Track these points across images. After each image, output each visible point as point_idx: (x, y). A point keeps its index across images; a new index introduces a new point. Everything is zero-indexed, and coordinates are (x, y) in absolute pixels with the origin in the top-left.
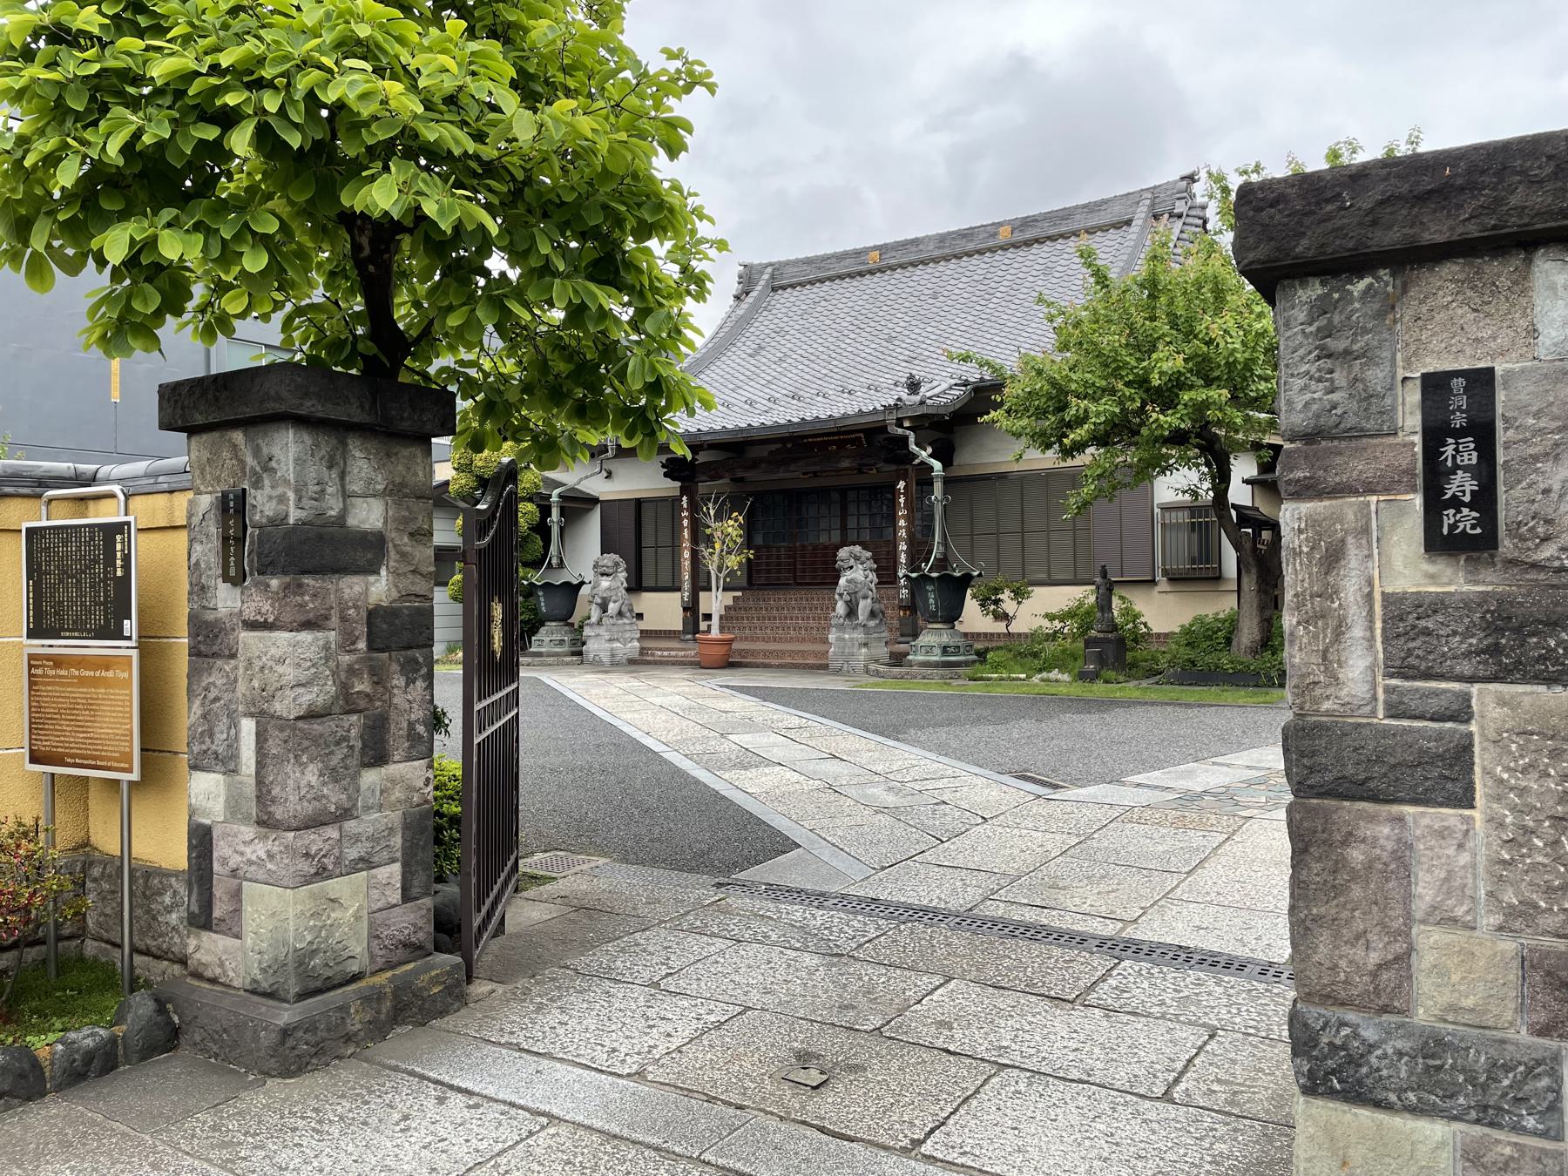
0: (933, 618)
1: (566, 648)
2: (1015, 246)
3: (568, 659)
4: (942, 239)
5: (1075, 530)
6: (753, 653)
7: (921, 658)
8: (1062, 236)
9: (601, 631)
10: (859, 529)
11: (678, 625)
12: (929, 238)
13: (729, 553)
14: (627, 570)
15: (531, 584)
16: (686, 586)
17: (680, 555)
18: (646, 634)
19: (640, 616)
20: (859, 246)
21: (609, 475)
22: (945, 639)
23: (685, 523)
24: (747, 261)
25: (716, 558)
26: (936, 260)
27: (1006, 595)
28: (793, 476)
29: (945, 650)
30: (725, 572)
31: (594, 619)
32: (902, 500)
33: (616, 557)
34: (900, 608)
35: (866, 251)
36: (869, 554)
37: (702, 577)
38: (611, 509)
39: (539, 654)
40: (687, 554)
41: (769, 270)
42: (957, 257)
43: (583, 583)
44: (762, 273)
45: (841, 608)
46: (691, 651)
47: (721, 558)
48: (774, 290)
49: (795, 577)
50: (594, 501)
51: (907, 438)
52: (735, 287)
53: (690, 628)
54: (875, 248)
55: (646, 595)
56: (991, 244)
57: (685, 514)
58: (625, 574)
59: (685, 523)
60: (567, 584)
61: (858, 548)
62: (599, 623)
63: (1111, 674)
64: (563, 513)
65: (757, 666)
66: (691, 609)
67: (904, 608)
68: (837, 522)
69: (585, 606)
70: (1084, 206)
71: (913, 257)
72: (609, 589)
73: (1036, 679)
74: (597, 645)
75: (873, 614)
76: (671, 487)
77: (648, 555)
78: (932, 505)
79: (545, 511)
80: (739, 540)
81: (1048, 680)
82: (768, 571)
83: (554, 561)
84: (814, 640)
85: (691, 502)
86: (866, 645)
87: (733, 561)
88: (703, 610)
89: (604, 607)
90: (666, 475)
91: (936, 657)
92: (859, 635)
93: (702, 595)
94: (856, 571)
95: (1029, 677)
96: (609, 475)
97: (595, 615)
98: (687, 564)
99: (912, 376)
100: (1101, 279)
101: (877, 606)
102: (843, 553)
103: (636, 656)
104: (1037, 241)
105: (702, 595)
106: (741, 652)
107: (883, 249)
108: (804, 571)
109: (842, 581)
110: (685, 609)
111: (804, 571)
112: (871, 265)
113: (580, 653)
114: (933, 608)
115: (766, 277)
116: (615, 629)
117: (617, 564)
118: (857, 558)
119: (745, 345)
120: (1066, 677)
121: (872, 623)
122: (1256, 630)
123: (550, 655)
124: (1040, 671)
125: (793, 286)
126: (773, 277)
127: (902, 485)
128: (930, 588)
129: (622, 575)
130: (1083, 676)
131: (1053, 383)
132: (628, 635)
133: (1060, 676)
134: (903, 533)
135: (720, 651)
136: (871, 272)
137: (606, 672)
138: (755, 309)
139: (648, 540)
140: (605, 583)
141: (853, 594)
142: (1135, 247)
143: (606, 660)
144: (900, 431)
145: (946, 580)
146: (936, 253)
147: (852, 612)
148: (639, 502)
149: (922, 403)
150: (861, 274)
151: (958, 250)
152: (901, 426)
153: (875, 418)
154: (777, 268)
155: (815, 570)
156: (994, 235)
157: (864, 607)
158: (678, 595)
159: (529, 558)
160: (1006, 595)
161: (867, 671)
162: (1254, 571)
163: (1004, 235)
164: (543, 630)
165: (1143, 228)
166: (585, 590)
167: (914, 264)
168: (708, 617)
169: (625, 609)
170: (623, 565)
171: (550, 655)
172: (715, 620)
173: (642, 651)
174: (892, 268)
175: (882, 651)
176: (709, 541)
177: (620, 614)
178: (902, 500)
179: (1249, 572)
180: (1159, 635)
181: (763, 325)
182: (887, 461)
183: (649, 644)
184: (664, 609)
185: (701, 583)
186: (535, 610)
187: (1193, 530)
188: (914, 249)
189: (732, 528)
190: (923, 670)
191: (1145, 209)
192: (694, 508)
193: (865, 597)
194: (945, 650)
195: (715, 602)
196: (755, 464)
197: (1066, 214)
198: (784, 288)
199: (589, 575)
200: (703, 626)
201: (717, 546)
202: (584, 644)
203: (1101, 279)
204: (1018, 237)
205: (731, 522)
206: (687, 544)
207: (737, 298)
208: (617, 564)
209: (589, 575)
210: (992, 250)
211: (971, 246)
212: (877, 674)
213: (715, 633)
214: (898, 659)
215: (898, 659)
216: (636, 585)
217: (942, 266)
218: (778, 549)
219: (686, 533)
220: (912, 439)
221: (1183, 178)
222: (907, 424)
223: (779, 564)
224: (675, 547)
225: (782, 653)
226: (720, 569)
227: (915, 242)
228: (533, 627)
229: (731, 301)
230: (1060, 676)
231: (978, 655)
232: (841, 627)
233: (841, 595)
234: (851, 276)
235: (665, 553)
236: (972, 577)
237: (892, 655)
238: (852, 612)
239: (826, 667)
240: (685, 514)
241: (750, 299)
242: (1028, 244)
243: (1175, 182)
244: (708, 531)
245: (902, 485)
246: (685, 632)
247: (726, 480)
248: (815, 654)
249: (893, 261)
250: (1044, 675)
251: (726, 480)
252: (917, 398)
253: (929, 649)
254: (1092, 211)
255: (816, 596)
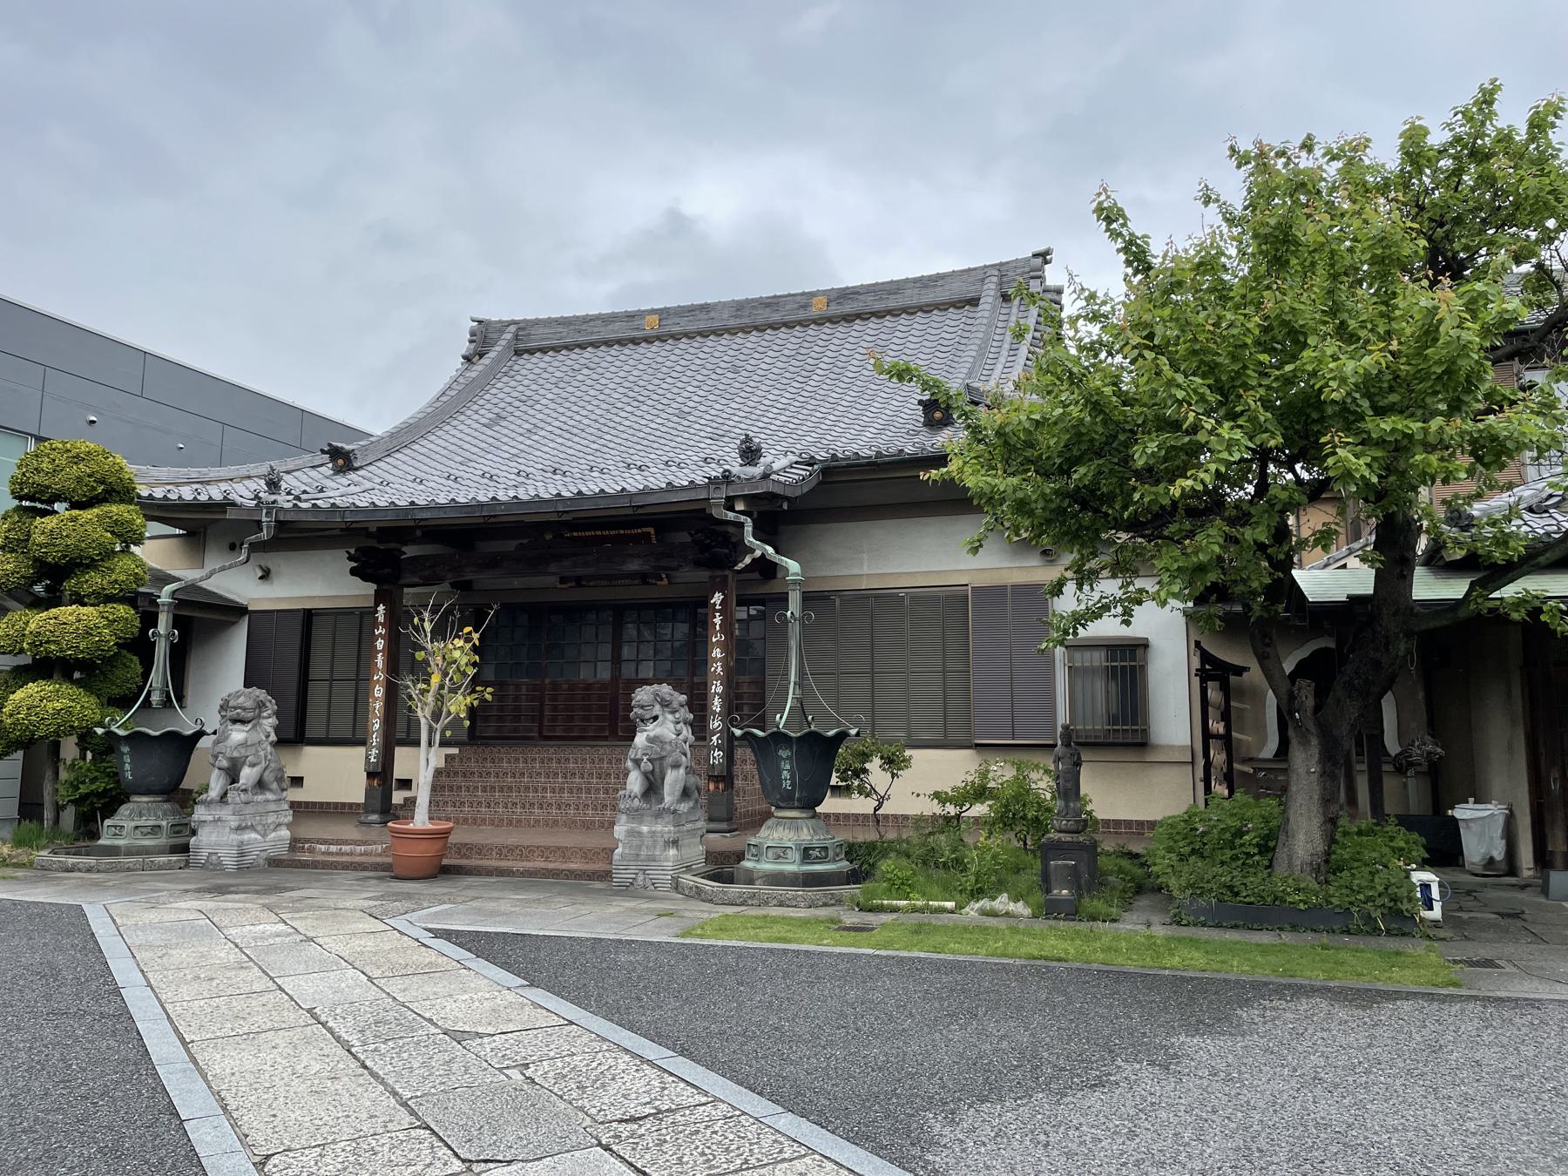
0: (786, 801)
1: (162, 840)
2: (832, 320)
3: (163, 859)
4: (740, 307)
5: (944, 672)
6: (481, 850)
7: (767, 866)
8: (890, 312)
9: (225, 813)
10: (638, 662)
11: (359, 796)
12: (724, 305)
13: (454, 691)
14: (278, 714)
15: (110, 734)
16: (375, 739)
17: (368, 692)
18: (302, 810)
19: (297, 781)
20: (632, 308)
21: (266, 575)
22: (806, 836)
23: (380, 644)
24: (481, 317)
25: (430, 698)
26: (732, 331)
27: (874, 765)
28: (546, 583)
29: (806, 854)
30: (444, 721)
31: (214, 793)
32: (717, 620)
33: (261, 694)
34: (711, 778)
35: (641, 314)
36: (683, 698)
37: (401, 725)
38: (263, 624)
39: (112, 851)
40: (379, 692)
41: (513, 328)
42: (759, 329)
43: (200, 734)
44: (503, 332)
45: (635, 782)
46: (373, 843)
47: (440, 698)
48: (518, 353)
49: (540, 733)
50: (239, 611)
51: (741, 525)
52: (465, 346)
53: (377, 804)
54: (653, 311)
55: (311, 752)
56: (801, 315)
57: (381, 631)
58: (273, 721)
59: (380, 644)
60: (173, 736)
61: (665, 689)
62: (223, 796)
63: (1098, 905)
64: (177, 622)
65: (501, 872)
66: (381, 775)
67: (716, 779)
68: (606, 651)
69: (204, 774)
70: (915, 280)
71: (702, 325)
72: (244, 744)
73: (972, 909)
74: (216, 835)
75: (686, 793)
76: (358, 592)
77: (317, 693)
78: (785, 622)
79: (150, 620)
80: (471, 671)
81: (993, 914)
82: (501, 719)
83: (156, 698)
84: (587, 826)
85: (390, 614)
86: (675, 843)
87: (459, 705)
88: (399, 772)
89: (232, 775)
90: (353, 572)
91: (792, 867)
92: (665, 828)
93: (400, 752)
94: (661, 725)
95: (960, 907)
96: (266, 575)
97: (216, 784)
98: (378, 707)
99: (748, 439)
100: (1136, 255)
101: (693, 779)
102: (642, 695)
103: (282, 851)
104: (859, 316)
105: (400, 752)
106: (466, 849)
107: (663, 313)
108: (554, 719)
109: (640, 739)
110: (370, 775)
111: (554, 719)
112: (648, 332)
113: (185, 849)
114: (787, 785)
115: (509, 336)
116: (249, 810)
117: (261, 705)
118: (665, 704)
119: (481, 411)
120: (1020, 908)
121: (684, 807)
122: (1317, 836)
123: (130, 852)
124: (977, 893)
125: (544, 350)
126: (516, 337)
127: (717, 598)
128: (784, 753)
129: (269, 723)
130: (1051, 910)
131: (1095, 405)
132: (271, 819)
133: (1012, 907)
134: (718, 668)
135: (426, 850)
136: (648, 340)
137: (221, 890)
138: (491, 375)
139: (319, 668)
140: (238, 735)
141: (658, 760)
142: (989, 326)
143: (229, 861)
144: (731, 515)
145: (813, 739)
146: (733, 322)
147: (652, 788)
148: (309, 616)
149: (765, 476)
150: (635, 341)
151: (760, 321)
152: (732, 509)
153: (693, 496)
154: (523, 328)
155: (571, 719)
156: (805, 307)
157: (673, 780)
158: (361, 750)
159: (116, 691)
160: (874, 765)
161: (677, 886)
162: (1315, 741)
163: (818, 307)
164: (124, 810)
165: (993, 311)
166: (205, 743)
167: (704, 334)
168: (406, 784)
169: (269, 777)
170: (272, 706)
171: (130, 852)
172: (422, 794)
173: (295, 844)
174: (676, 337)
175: (695, 852)
176: (421, 671)
177: (261, 785)
178: (717, 620)
179: (1305, 743)
180: (1107, 822)
181: (502, 392)
182: (699, 564)
183: (312, 829)
184: (336, 773)
185: (400, 732)
186: (116, 776)
187: (1114, 676)
188: (703, 316)
189: (459, 650)
190: (780, 891)
191: (993, 286)
192: (397, 619)
193: (676, 766)
194: (806, 854)
195: (420, 765)
196: (493, 562)
197: (895, 287)
198: (531, 352)
199: (212, 721)
200: (398, 797)
201: (435, 680)
202: (194, 833)
203: (1136, 255)
204: (835, 310)
205: (459, 643)
206: (379, 676)
207: (468, 359)
208: (261, 705)
209: (212, 721)
210: (803, 324)
211: (776, 317)
212: (698, 894)
213: (421, 820)
214: (723, 867)
215: (723, 867)
216: (294, 735)
217: (739, 338)
218: (518, 687)
219: (380, 660)
220: (749, 528)
221: (1035, 256)
222: (740, 507)
223: (518, 709)
224: (361, 682)
225: (524, 852)
226: (436, 716)
227: (705, 308)
228: (111, 801)
229: (459, 362)
230: (1012, 907)
231: (861, 863)
232: (636, 815)
233: (637, 762)
234: (621, 342)
235: (344, 691)
236: (848, 735)
237: (710, 856)
238: (652, 788)
239: (606, 876)
240: (381, 631)
241: (486, 361)
242: (849, 318)
243: (1027, 260)
244: (420, 655)
245: (717, 598)
246: (367, 807)
247: (446, 586)
248: (586, 854)
249: (676, 329)
250: (985, 903)
251: (446, 586)
252: (757, 471)
253: (781, 853)
254: (926, 287)
255: (582, 759)
